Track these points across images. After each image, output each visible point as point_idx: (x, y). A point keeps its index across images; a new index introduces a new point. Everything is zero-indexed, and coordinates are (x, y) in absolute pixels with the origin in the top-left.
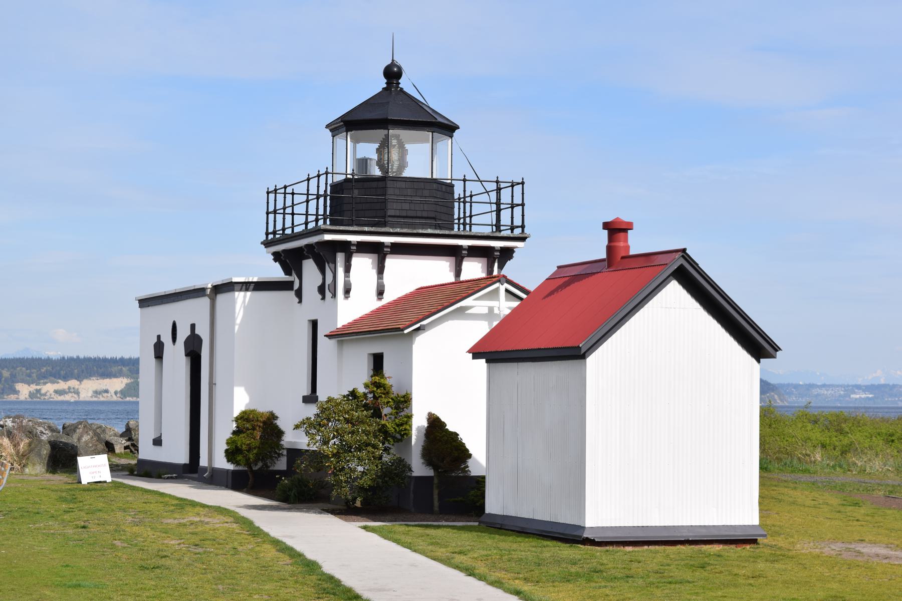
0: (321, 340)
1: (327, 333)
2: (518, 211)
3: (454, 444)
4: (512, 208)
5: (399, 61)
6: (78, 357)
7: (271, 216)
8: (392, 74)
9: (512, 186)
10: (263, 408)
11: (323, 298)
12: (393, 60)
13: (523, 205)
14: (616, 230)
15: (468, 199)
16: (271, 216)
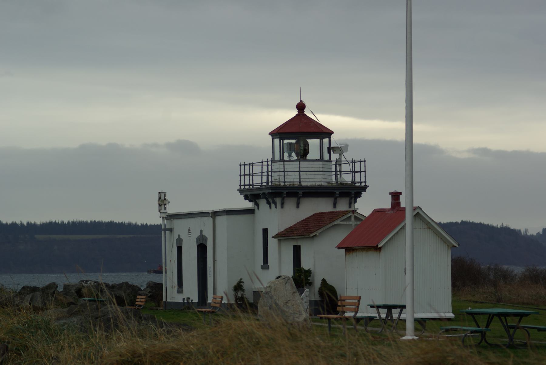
0: (272, 243)
1: (274, 234)
5: (305, 102)
7: (242, 177)
11: (271, 208)
12: (301, 101)
13: (365, 172)
16: (242, 177)
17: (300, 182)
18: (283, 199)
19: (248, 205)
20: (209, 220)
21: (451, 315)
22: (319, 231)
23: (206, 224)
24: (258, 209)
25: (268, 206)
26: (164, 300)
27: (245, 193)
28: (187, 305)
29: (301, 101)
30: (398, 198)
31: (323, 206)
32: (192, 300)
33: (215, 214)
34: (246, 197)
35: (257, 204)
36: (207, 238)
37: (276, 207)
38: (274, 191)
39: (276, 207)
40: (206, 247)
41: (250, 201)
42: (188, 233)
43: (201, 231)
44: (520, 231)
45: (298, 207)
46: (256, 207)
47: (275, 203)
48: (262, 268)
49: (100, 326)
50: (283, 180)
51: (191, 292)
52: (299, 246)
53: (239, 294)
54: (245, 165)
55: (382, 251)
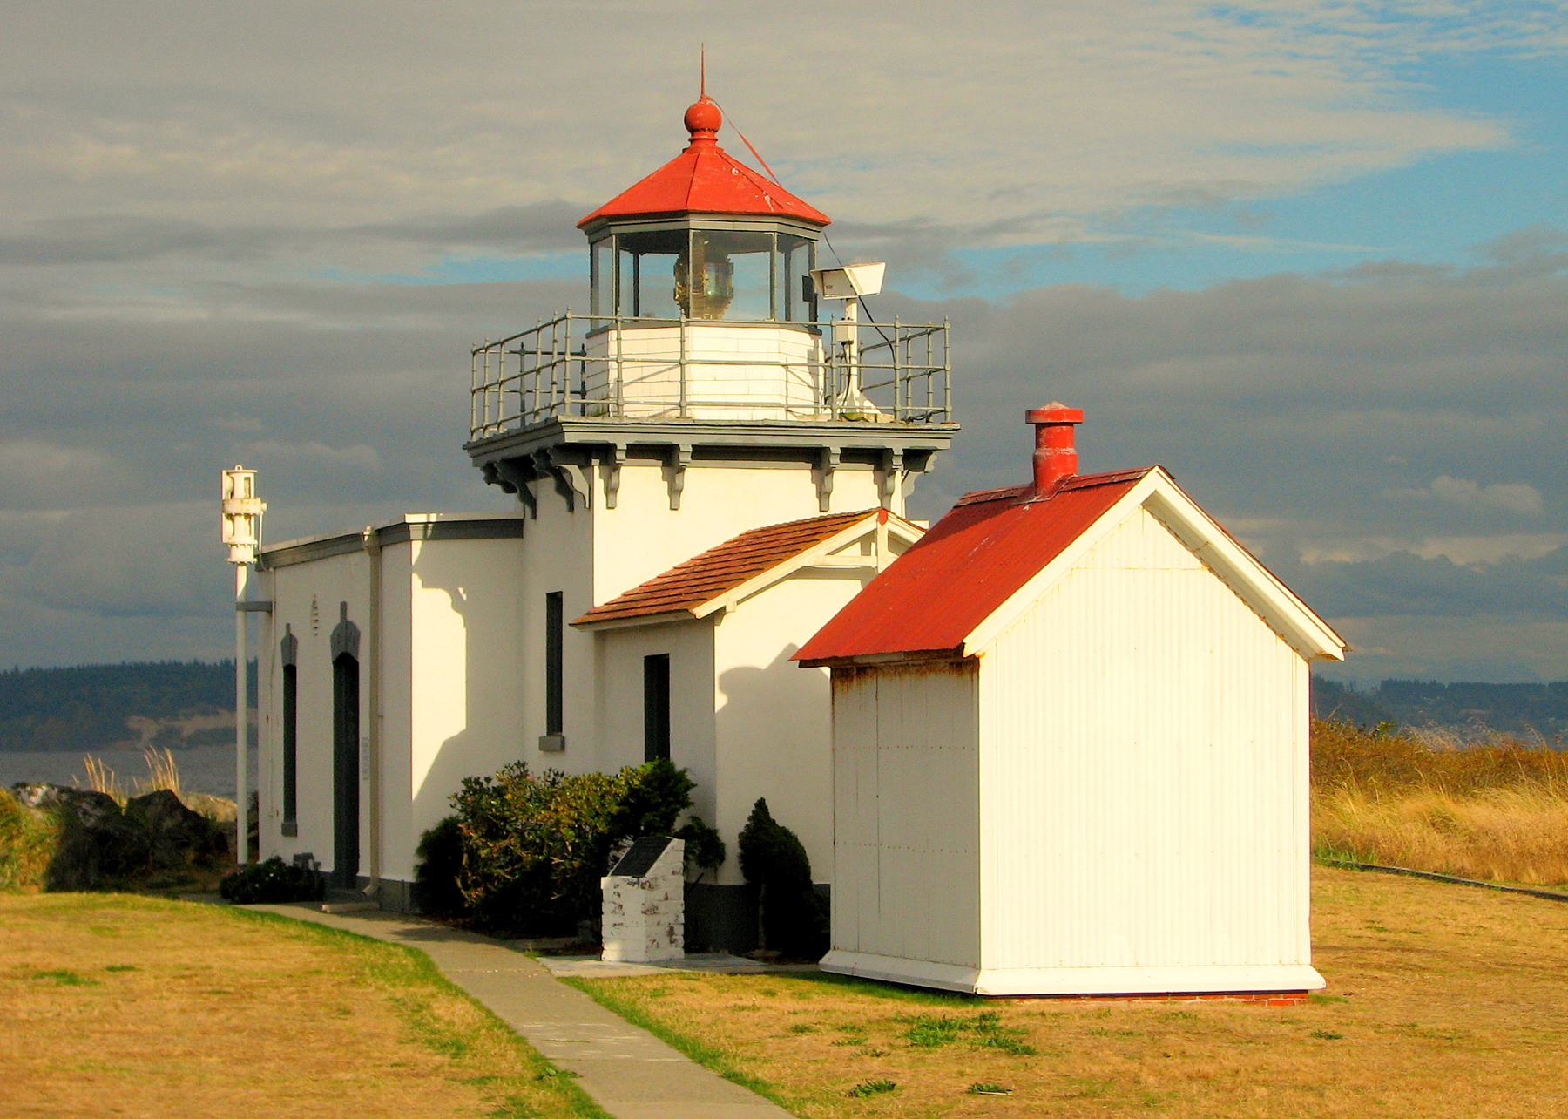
0: (576, 643)
19: (505, 505)
21: (1313, 981)
24: (534, 516)
26: (242, 858)
27: (485, 459)
32: (318, 864)
34: (491, 474)
35: (530, 501)
40: (357, 664)
41: (509, 488)
43: (344, 606)
44: (1341, 685)
45: (761, 805)
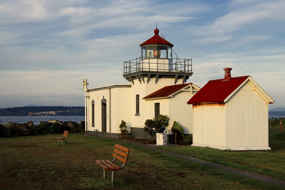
0: (142, 102)
2: (190, 67)
3: (52, 126)
4: (188, 66)
6: (45, 106)
8: (157, 32)
9: (188, 61)
10: (169, 117)
11: (141, 83)
12: (157, 29)
14: (228, 70)
15: (137, 69)
17: (158, 69)
18: (149, 78)
20: (108, 90)
22: (173, 94)
23: (105, 93)
25: (140, 82)
27: (126, 77)
28: (97, 132)
29: (157, 29)
30: (229, 72)
31: (170, 82)
33: (110, 88)
34: (127, 79)
36: (106, 100)
37: (144, 83)
38: (143, 74)
39: (144, 83)
42: (97, 97)
43: (104, 97)
46: (132, 83)
47: (143, 80)
48: (136, 115)
49: (72, 128)
50: (149, 68)
51: (98, 127)
52: (159, 104)
53: (124, 128)
54: (126, 62)
55: (226, 104)
